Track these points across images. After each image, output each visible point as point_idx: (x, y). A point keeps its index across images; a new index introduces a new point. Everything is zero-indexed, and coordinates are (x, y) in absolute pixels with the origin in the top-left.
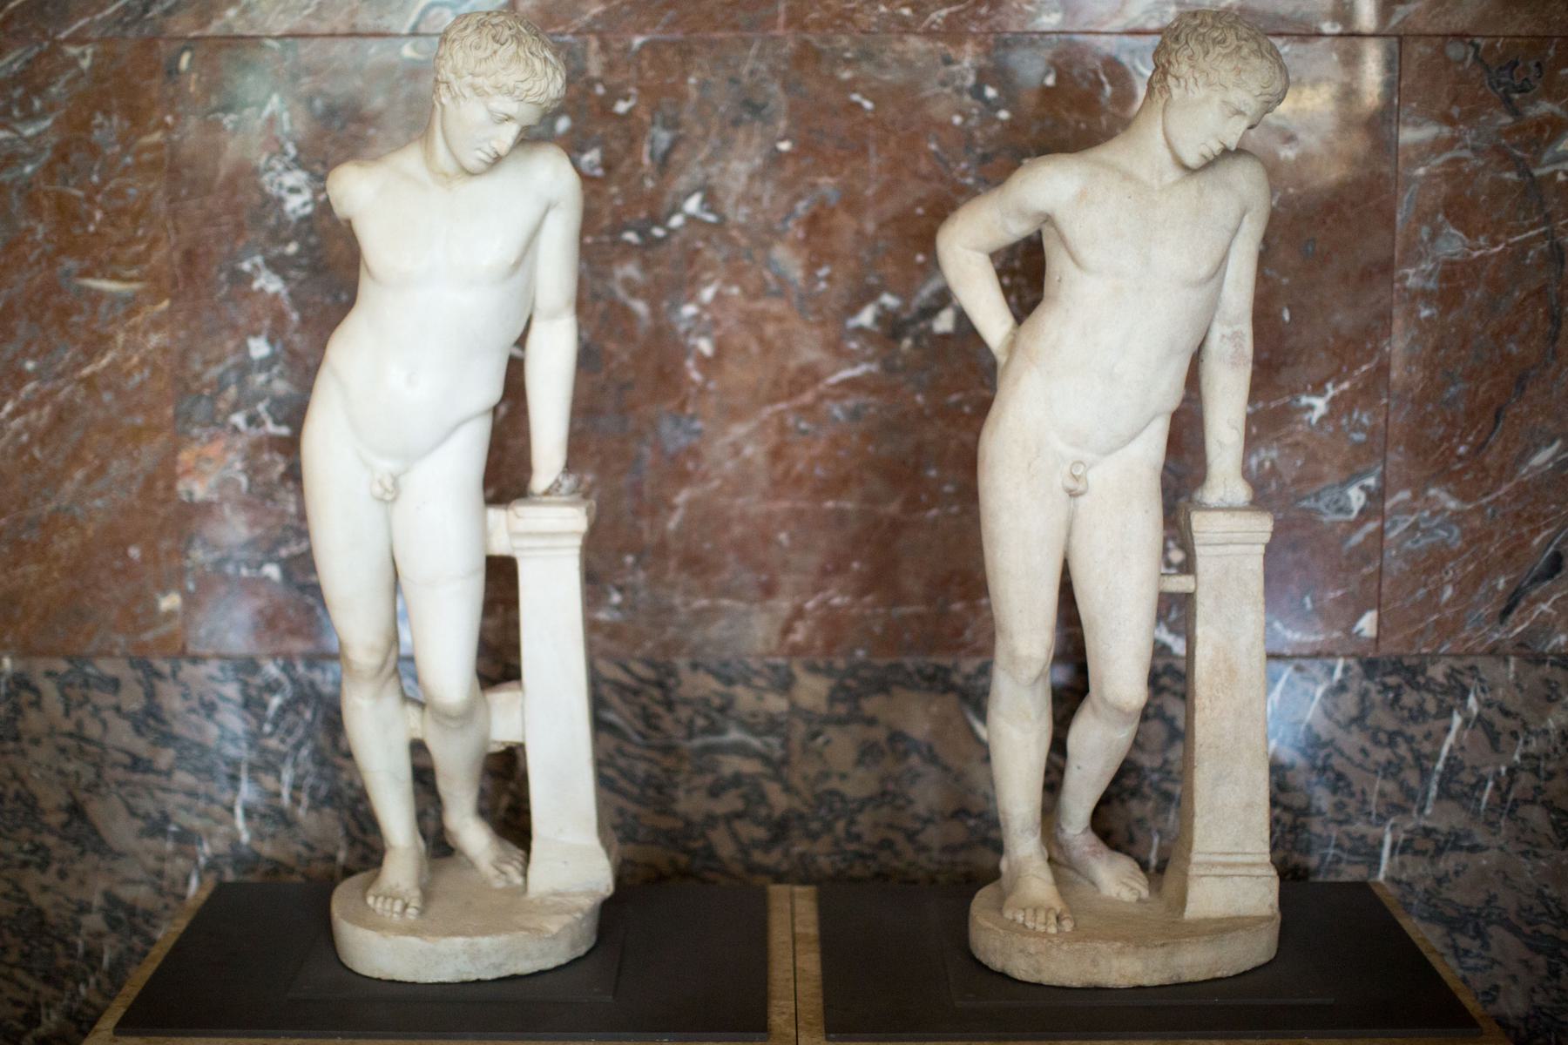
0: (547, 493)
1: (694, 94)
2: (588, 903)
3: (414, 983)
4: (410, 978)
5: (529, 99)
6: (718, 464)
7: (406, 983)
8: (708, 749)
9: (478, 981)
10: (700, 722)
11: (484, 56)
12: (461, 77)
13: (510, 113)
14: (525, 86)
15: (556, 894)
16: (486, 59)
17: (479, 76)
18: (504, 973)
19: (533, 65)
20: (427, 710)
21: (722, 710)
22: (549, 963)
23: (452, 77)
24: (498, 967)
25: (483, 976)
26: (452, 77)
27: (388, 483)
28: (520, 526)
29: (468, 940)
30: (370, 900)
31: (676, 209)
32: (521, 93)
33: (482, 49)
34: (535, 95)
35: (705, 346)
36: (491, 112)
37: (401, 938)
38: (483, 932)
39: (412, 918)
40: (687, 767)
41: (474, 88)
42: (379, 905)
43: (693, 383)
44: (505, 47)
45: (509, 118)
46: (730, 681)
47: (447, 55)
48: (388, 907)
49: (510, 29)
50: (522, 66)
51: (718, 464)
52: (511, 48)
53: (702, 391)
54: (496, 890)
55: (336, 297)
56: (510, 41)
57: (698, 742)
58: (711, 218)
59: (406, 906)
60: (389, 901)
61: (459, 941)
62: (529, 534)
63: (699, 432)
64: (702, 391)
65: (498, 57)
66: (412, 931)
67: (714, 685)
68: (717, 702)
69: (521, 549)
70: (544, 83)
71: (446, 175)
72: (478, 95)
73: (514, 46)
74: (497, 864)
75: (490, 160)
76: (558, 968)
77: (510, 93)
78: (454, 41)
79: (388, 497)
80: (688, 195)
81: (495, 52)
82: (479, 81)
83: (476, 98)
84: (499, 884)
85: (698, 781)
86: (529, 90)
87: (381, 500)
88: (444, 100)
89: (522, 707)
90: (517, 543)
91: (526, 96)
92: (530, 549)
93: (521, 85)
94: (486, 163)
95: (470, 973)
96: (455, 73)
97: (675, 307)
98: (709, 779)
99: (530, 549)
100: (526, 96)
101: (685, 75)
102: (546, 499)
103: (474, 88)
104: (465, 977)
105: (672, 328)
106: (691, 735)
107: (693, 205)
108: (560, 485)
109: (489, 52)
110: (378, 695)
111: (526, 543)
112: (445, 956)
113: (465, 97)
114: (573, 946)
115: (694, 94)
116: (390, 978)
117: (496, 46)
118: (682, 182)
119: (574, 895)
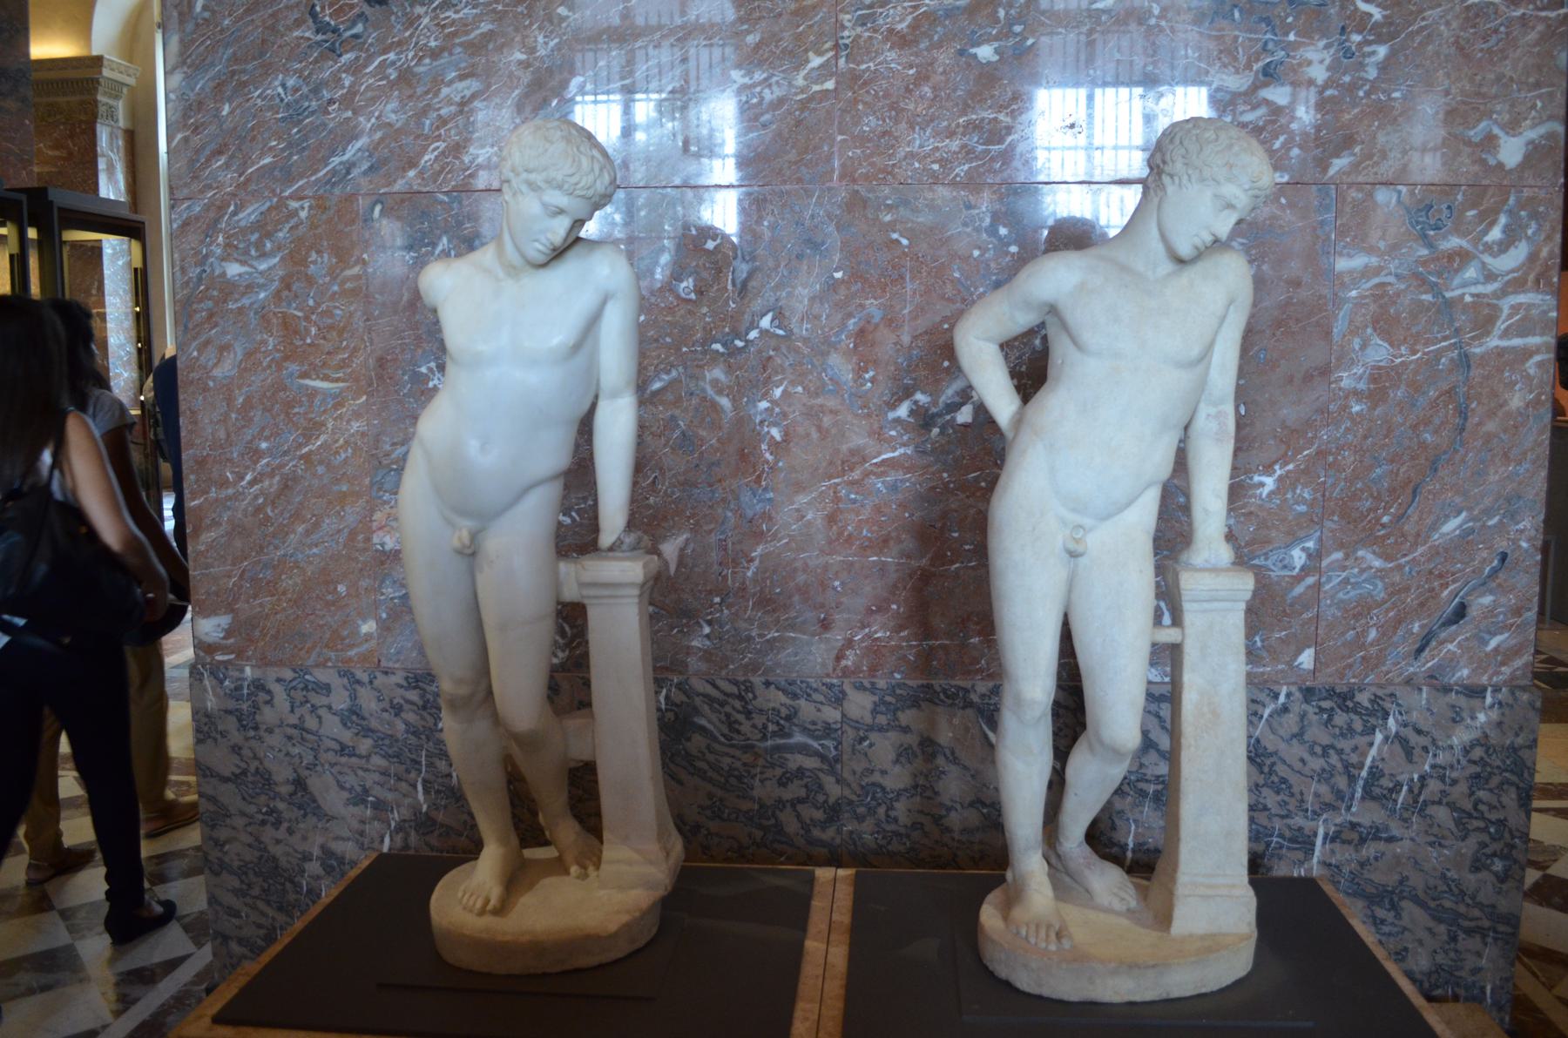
0: (611, 549)
8: (778, 748)
10: (771, 727)
14: (574, 180)
21: (788, 718)
28: (587, 577)
34: (582, 188)
36: (545, 205)
40: (761, 762)
43: (767, 462)
46: (795, 696)
57: (769, 743)
58: (781, 332)
67: (783, 699)
68: (784, 712)
69: (589, 597)
71: (514, 268)
72: (533, 190)
77: (560, 187)
82: (533, 177)
83: (532, 194)
93: (568, 179)
98: (779, 772)
102: (610, 554)
106: (764, 738)
118: (757, 305)
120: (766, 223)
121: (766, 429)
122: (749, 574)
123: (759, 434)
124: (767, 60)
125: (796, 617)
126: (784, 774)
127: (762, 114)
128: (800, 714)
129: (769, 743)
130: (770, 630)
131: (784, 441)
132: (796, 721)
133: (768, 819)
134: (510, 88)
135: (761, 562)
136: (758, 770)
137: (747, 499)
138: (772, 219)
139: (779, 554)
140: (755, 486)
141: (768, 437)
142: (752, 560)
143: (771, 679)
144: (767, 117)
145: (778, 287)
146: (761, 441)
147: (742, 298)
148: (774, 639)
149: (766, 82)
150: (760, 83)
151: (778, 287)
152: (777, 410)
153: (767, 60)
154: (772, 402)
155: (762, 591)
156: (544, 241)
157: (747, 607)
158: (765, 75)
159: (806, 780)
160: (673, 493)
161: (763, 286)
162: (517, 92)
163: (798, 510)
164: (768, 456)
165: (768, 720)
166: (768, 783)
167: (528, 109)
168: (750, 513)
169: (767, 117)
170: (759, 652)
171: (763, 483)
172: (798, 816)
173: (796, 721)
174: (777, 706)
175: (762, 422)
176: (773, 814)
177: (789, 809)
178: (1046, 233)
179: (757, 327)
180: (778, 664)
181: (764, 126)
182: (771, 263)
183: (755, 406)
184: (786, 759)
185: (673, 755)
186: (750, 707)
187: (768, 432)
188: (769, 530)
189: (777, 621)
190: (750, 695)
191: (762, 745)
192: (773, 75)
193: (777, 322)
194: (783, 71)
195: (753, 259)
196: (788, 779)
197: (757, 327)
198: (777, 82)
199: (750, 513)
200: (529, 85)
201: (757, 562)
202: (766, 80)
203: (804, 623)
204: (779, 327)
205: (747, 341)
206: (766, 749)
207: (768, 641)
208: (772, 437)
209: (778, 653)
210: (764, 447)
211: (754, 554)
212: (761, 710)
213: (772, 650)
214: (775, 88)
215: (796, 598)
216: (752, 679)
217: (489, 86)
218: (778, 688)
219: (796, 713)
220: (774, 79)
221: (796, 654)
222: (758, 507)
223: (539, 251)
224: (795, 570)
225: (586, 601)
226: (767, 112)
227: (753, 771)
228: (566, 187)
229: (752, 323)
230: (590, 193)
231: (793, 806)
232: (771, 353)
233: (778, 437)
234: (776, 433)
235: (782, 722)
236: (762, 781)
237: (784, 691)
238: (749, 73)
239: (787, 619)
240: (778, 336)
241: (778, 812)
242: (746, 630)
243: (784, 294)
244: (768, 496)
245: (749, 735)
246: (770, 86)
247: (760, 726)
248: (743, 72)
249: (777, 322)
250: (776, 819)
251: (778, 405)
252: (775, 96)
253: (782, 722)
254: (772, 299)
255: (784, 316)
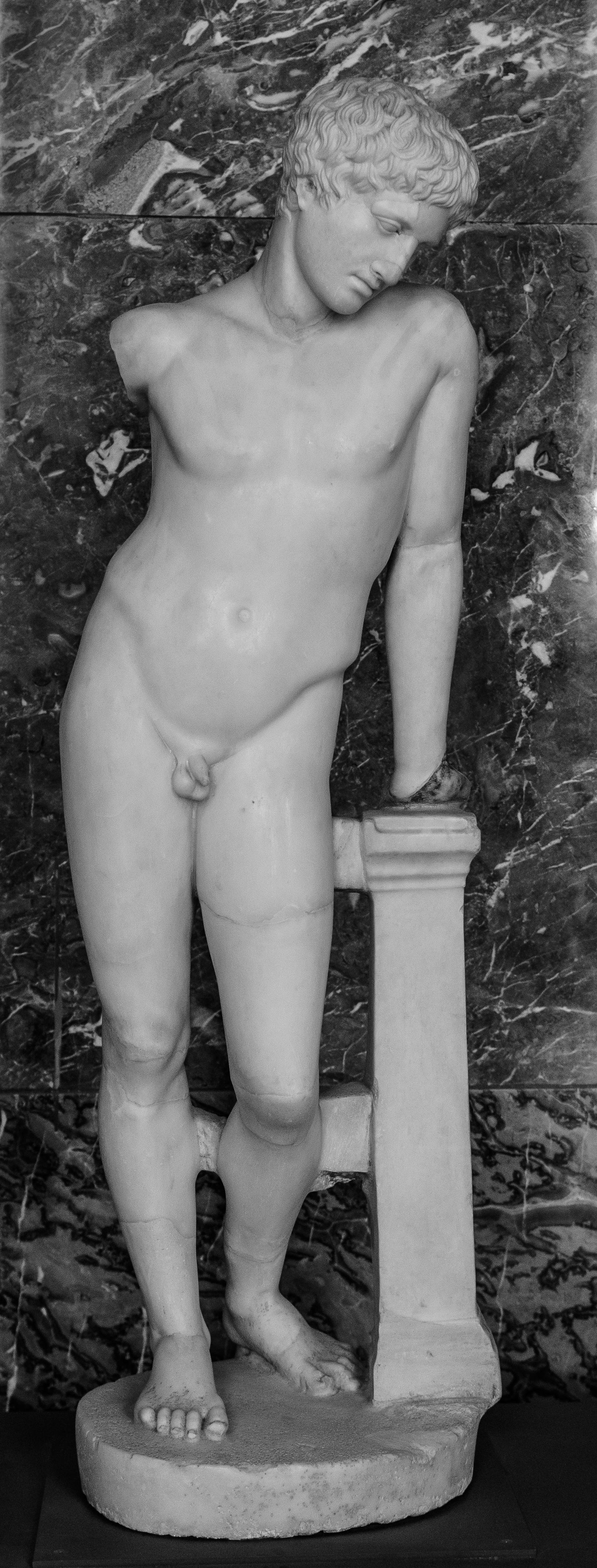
0: (417, 798)
1: (530, 308)
2: (472, 1414)
3: (225, 1540)
4: (217, 1535)
5: (436, 198)
6: (558, 815)
7: (211, 1540)
8: (539, 1217)
9: (322, 1534)
10: (530, 1179)
11: (371, 132)
12: (334, 165)
13: (406, 218)
14: (432, 177)
15: (417, 1401)
16: (375, 136)
17: (362, 161)
18: (359, 1521)
19: (442, 149)
20: (235, 1121)
21: (559, 1161)
22: (422, 1507)
23: (318, 165)
24: (350, 1511)
25: (329, 1527)
26: (318, 165)
27: (200, 770)
28: (382, 844)
29: (311, 1469)
30: (147, 1416)
31: (502, 466)
32: (425, 188)
33: (367, 123)
34: (445, 192)
35: (541, 652)
36: (377, 216)
37: (209, 1468)
38: (331, 1455)
39: (215, 1438)
40: (510, 1243)
41: (353, 180)
42: (163, 1422)
43: (526, 702)
44: (402, 119)
45: (403, 227)
46: (572, 1121)
47: (312, 133)
48: (178, 1422)
49: (405, 99)
50: (428, 147)
51: (558, 815)
52: (410, 122)
53: (537, 714)
54: (321, 1400)
55: (30, 578)
56: (407, 114)
57: (526, 1207)
58: (552, 477)
59: (204, 1423)
60: (179, 1414)
61: (297, 1471)
62: (394, 856)
63: (531, 770)
64: (537, 714)
65: (392, 133)
66: (220, 1457)
67: (551, 1125)
68: (552, 1149)
69: (381, 879)
70: (456, 175)
71: (295, 319)
72: (359, 191)
73: (415, 118)
74: (317, 1361)
75: (367, 292)
76: (434, 1513)
77: (408, 187)
78: (322, 114)
79: (199, 793)
80: (521, 447)
81: (388, 127)
82: (362, 169)
83: (354, 195)
84: (324, 1391)
85: (525, 1264)
86: (435, 184)
87: (189, 800)
88: (302, 203)
89: (372, 1117)
90: (375, 870)
91: (432, 192)
92: (394, 878)
93: (425, 175)
94: (373, 290)
95: (311, 1521)
96: (324, 160)
97: (501, 597)
98: (542, 1260)
99: (394, 878)
100: (432, 192)
101: (518, 281)
102: (414, 807)
103: (353, 180)
104: (303, 1529)
105: (497, 627)
106: (516, 1199)
107: (526, 459)
108: (438, 786)
109: (378, 127)
110: (160, 1101)
111: (389, 869)
112: (274, 1494)
113: (338, 196)
114: (453, 1480)
115: (530, 308)
116: (187, 1534)
117: (388, 119)
118: (511, 429)
119: (442, 1401)
120: (527, 288)
121: (524, 645)
122: (492, 901)
123: (512, 652)
124: (533, 8)
125: (573, 978)
126: (551, 1264)
127: (524, 100)
128: (580, 1153)
129: (526, 1207)
130: (527, 1003)
131: (555, 665)
132: (573, 1166)
133: (522, 1350)
134: (75, 33)
135: (511, 881)
136: (506, 1257)
137: (489, 767)
138: (539, 281)
139: (545, 866)
140: (503, 745)
141: (528, 658)
142: (498, 876)
143: (529, 1091)
144: (531, 106)
145: (550, 397)
146: (517, 665)
147: (485, 417)
148: (534, 1016)
149: (530, 46)
150: (519, 48)
151: (550, 397)
152: (544, 611)
153: (533, 8)
154: (535, 597)
155: (513, 933)
156: (368, 275)
157: (487, 960)
158: (529, 34)
159: (590, 1274)
160: (359, 757)
161: (522, 396)
162: (88, 41)
163: (578, 787)
164: (527, 691)
165: (523, 1165)
166: (522, 1282)
167: (108, 73)
168: (494, 793)
169: (531, 106)
170: (507, 1042)
171: (519, 740)
172: (576, 1342)
173: (573, 1166)
174: (540, 1138)
175: (517, 633)
176: (532, 1341)
177: (559, 1329)
178: (49, 488)
179: (512, 467)
180: (542, 1065)
181: (527, 121)
182: (536, 358)
183: (507, 605)
184: (557, 1237)
185: (350, 1236)
186: (492, 1142)
187: (529, 650)
188: (527, 824)
189: (541, 985)
190: (492, 1121)
191: (512, 1211)
192: (543, 34)
193: (545, 459)
194: (562, 29)
195: (506, 349)
196: (558, 1273)
197: (512, 467)
198: (550, 48)
199: (494, 793)
200: (109, 31)
201: (505, 881)
202: (530, 42)
203: (587, 987)
204: (549, 468)
205: (493, 492)
206: (519, 1218)
207: (523, 1021)
208: (535, 659)
209: (539, 1046)
210: (520, 676)
211: (500, 866)
212: (512, 1148)
213: (530, 1038)
214: (545, 57)
215: (574, 944)
216: (496, 1092)
217: (38, 27)
218: (542, 1107)
219: (572, 1152)
220: (546, 41)
221: (572, 1046)
222: (508, 782)
223: (357, 293)
224: (573, 893)
225: (374, 886)
226: (531, 97)
227: (496, 1262)
228: (419, 187)
229: (502, 459)
230: (452, 199)
231: (567, 1323)
232: (535, 512)
233: (545, 660)
234: (541, 652)
235: (548, 1168)
236: (511, 1279)
237: (552, 1111)
238: (502, 29)
239: (556, 982)
240: (547, 482)
241: (539, 1336)
242: (486, 1002)
243: (558, 411)
244: (526, 763)
245: (489, 1194)
246: (537, 53)
247: (509, 1177)
248: (491, 27)
249: (545, 459)
250: (536, 1349)
251: (545, 603)
252: (545, 71)
253: (548, 1168)
254: (538, 418)
255: (557, 447)
